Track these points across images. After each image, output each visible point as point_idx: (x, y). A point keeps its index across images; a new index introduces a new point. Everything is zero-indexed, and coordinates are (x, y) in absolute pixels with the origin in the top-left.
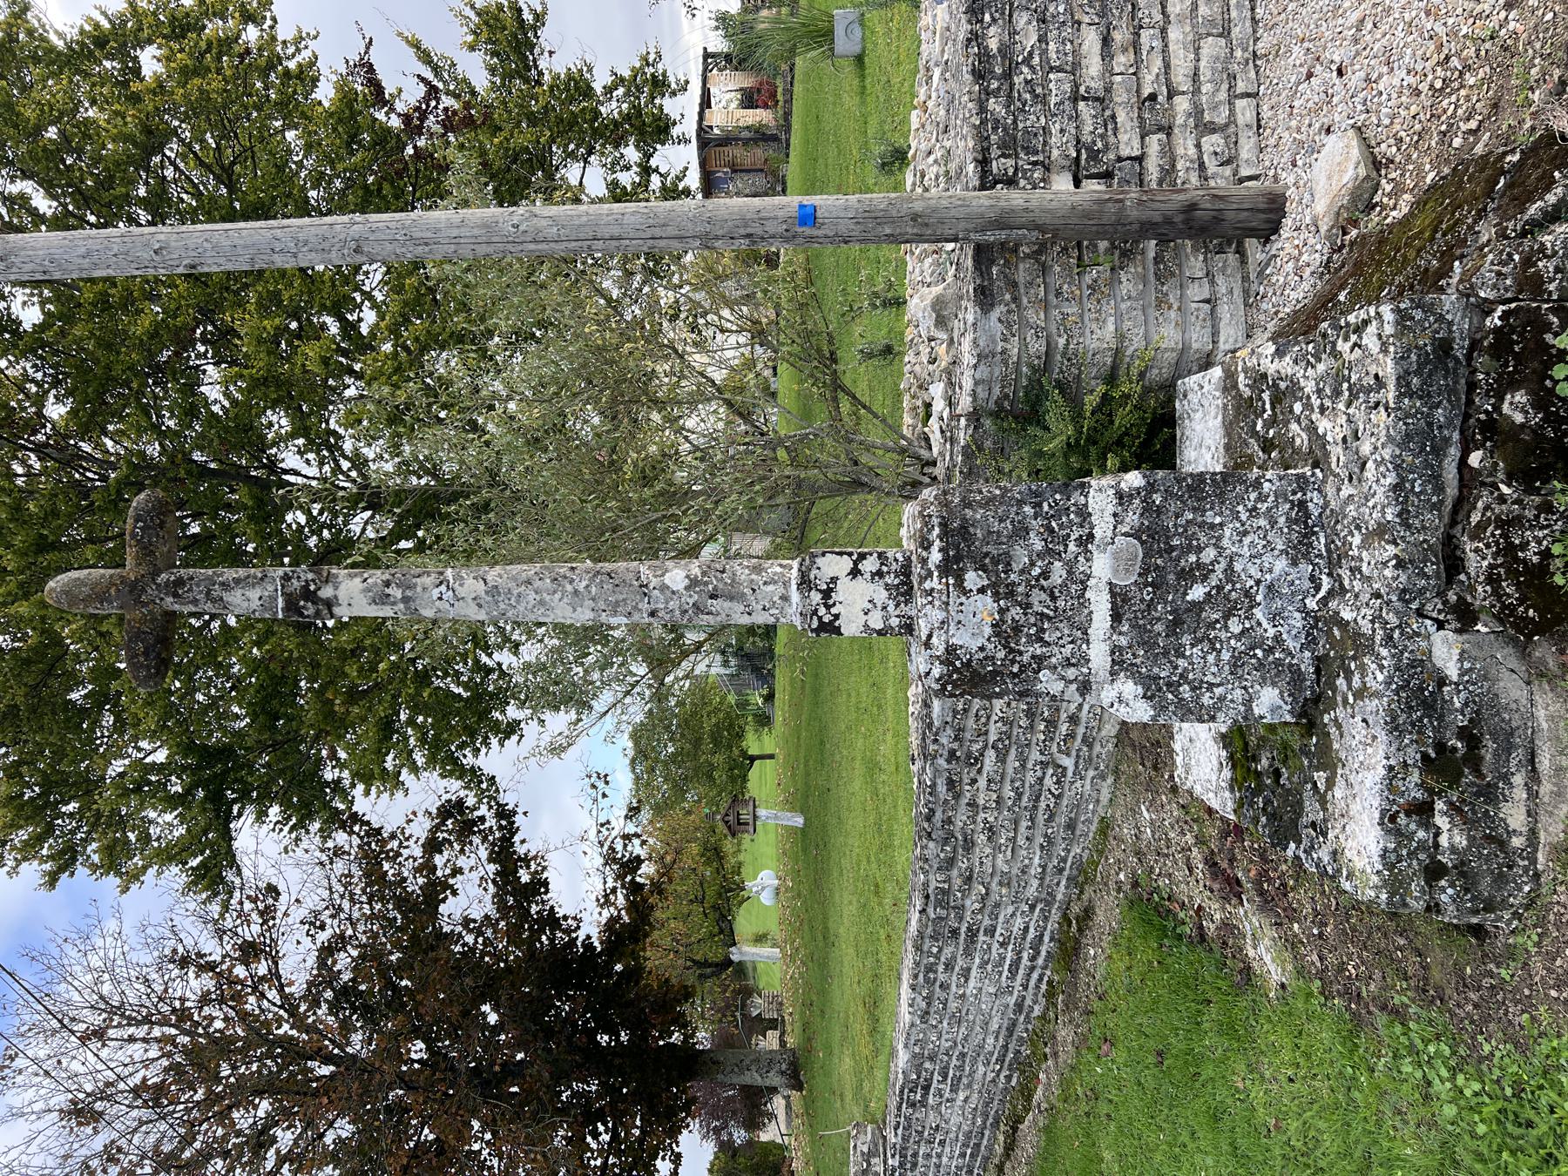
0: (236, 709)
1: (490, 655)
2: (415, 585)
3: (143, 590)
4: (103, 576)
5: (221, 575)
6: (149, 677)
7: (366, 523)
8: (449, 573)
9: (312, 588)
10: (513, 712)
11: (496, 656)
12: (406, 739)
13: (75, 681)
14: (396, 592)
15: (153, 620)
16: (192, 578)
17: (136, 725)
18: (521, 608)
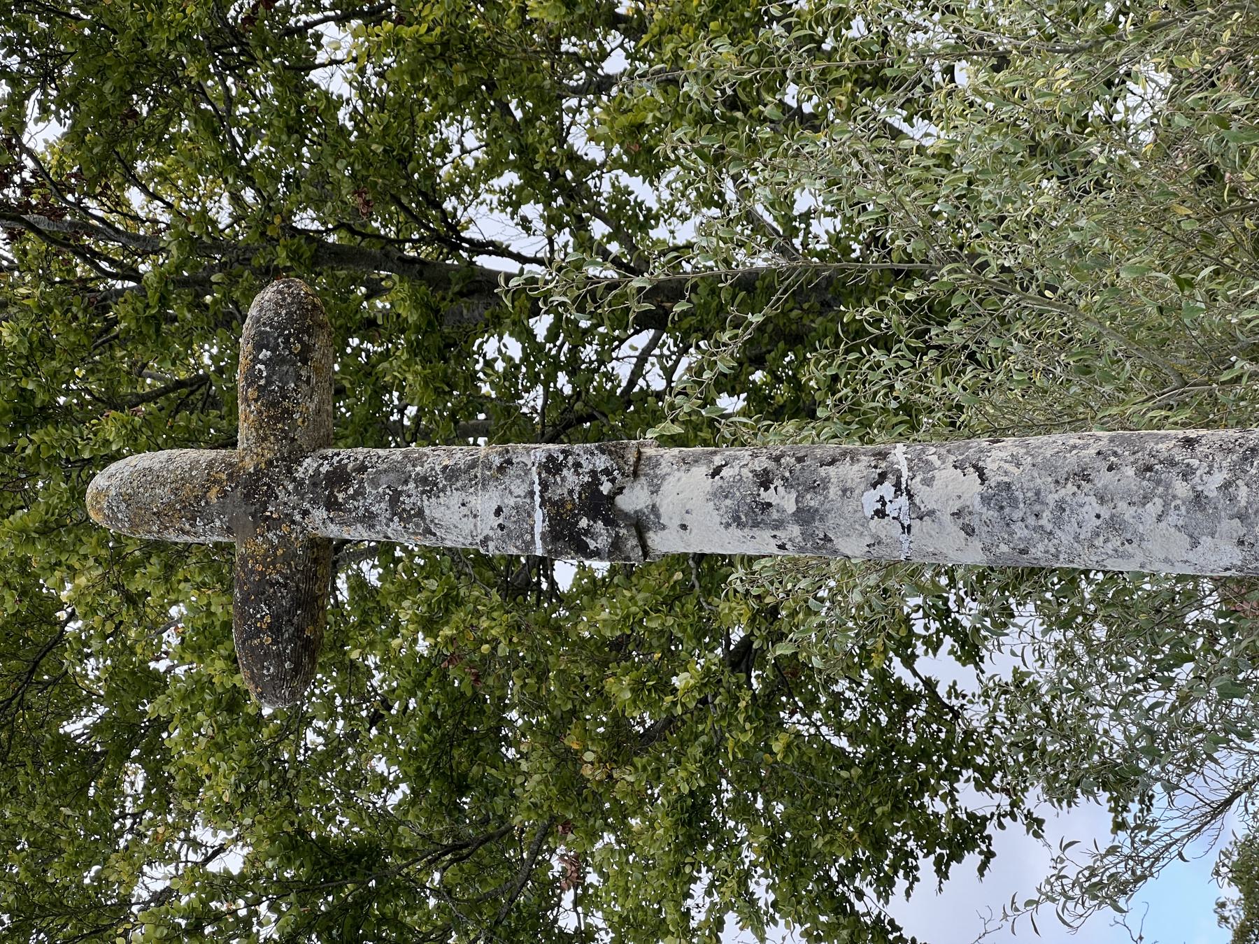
0: (381, 766)
1: (909, 661)
2: (826, 482)
3: (270, 494)
4: (194, 465)
5: (419, 461)
6: (281, 678)
7: (642, 359)
8: (899, 455)
9: (606, 488)
10: (971, 799)
11: (925, 665)
12: (735, 848)
13: (77, 702)
14: (783, 499)
15: (289, 557)
16: (362, 468)
17: (191, 793)
18: (1064, 537)
